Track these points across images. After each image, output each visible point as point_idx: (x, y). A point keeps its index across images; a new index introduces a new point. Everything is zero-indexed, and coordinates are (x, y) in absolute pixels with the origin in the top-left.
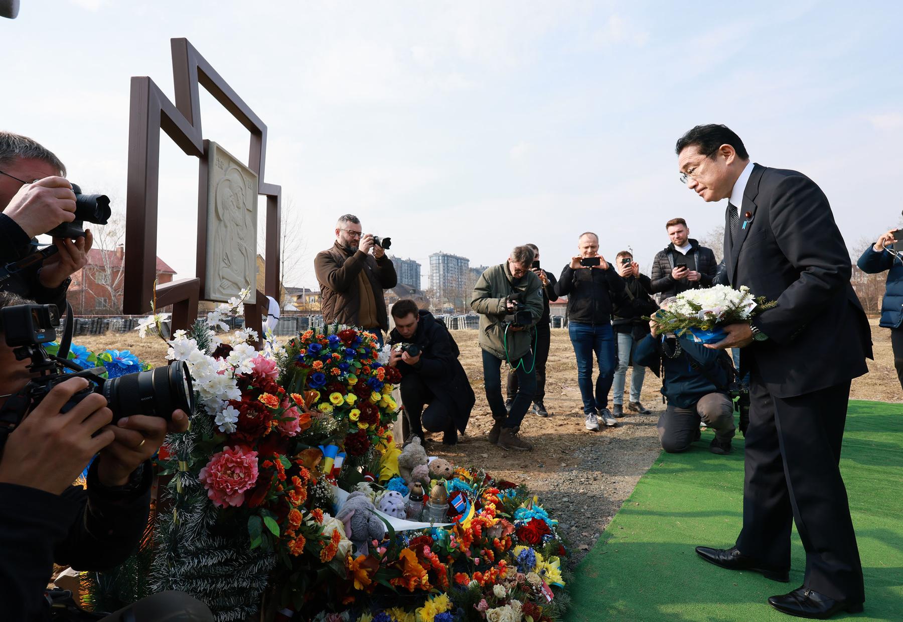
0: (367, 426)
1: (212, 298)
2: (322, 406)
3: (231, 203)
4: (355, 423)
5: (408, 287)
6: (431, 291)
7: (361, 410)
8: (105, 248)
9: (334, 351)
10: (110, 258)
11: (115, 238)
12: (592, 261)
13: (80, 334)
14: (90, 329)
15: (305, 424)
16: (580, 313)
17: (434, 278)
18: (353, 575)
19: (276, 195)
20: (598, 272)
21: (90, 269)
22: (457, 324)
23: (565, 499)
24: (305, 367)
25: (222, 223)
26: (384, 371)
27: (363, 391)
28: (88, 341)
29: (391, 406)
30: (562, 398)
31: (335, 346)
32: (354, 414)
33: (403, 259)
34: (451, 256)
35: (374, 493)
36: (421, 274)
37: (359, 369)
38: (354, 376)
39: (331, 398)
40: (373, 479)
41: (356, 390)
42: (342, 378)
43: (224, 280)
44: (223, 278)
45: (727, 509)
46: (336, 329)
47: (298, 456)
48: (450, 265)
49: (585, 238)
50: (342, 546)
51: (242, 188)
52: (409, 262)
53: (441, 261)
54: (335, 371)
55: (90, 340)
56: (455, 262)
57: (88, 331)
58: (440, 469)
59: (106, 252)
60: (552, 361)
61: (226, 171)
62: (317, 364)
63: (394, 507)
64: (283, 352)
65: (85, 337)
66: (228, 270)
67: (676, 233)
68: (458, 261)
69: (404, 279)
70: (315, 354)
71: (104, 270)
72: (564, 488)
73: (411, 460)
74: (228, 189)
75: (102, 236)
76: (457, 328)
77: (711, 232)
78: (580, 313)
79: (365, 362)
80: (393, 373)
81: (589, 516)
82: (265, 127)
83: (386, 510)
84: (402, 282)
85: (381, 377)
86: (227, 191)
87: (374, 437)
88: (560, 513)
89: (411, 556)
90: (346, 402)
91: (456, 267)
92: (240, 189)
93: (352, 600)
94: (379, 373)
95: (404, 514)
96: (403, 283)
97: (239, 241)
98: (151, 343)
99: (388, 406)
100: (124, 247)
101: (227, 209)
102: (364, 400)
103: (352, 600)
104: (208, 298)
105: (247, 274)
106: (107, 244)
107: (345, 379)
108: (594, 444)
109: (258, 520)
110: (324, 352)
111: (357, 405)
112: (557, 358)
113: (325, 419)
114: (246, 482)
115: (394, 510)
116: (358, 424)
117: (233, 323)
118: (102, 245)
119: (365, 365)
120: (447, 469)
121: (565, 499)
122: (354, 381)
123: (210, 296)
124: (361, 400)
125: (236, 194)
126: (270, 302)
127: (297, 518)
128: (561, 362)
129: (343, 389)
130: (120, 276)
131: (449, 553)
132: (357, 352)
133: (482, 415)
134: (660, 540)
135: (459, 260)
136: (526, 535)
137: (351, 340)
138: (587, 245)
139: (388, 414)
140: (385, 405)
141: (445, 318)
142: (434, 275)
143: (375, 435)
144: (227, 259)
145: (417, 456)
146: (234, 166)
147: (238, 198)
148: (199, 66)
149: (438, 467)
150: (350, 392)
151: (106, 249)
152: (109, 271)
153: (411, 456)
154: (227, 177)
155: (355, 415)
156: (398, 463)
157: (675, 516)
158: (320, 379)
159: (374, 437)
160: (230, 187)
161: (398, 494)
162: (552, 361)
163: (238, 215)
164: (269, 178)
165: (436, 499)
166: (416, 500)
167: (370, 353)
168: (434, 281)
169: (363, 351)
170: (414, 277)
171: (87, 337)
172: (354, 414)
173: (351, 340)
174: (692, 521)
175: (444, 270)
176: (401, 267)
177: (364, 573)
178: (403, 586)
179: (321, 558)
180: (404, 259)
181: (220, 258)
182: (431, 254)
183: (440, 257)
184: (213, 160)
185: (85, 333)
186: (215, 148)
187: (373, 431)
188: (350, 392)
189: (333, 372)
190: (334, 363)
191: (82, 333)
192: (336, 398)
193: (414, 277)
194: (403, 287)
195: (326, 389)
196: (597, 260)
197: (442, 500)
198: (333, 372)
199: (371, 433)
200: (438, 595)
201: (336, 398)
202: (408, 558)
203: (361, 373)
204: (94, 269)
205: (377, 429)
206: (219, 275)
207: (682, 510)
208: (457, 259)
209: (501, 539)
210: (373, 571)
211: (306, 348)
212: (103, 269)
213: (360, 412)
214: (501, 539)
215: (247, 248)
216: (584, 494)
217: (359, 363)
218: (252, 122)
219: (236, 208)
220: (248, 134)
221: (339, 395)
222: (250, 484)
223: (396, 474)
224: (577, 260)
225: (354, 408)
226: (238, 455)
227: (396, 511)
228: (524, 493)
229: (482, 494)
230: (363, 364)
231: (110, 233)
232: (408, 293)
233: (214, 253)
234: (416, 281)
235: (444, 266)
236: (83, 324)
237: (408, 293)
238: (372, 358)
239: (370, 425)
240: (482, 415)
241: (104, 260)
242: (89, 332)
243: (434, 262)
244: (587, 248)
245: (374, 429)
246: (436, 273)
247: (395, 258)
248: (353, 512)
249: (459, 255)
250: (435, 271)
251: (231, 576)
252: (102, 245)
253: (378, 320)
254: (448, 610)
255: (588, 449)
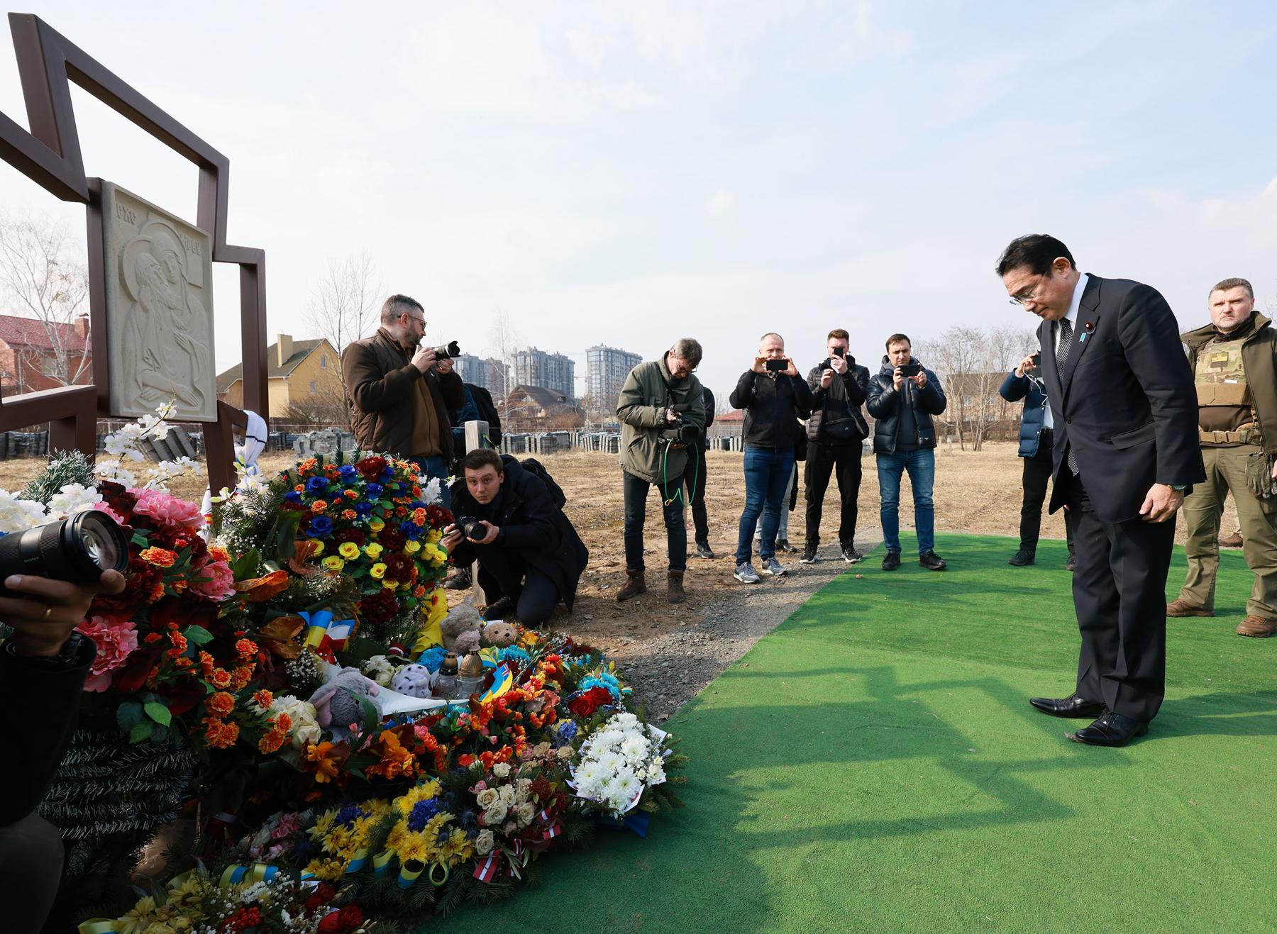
0: (397, 584)
1: (122, 414)
2: (327, 561)
3: (155, 276)
4: (379, 582)
5: (555, 393)
6: (589, 400)
7: (387, 564)
8: (50, 318)
9: (350, 487)
10: (61, 336)
11: (69, 304)
12: (778, 364)
13: (15, 457)
14: (34, 449)
15: (280, 584)
16: (761, 435)
17: (594, 381)
18: (315, 766)
19: (253, 262)
20: (783, 378)
21: (27, 352)
22: (617, 446)
23: (665, 664)
24: (297, 508)
25: (138, 306)
26: (425, 513)
27: (393, 541)
28: (26, 467)
29: (438, 558)
30: (720, 542)
31: (350, 480)
32: (377, 571)
33: (548, 353)
34: (617, 352)
35: (393, 668)
36: (575, 375)
37: (392, 510)
38: (379, 520)
39: (342, 550)
40: (402, 652)
41: (382, 538)
42: (360, 522)
43: (148, 388)
44: (145, 385)
45: (845, 666)
46: (357, 457)
47: (268, 627)
48: (616, 364)
49: (769, 339)
50: (303, 733)
51: (178, 254)
52: (557, 357)
53: (602, 358)
54: (348, 513)
55: (29, 466)
56: (622, 359)
57: (29, 451)
58: (498, 635)
59: (55, 327)
60: (726, 496)
61: (140, 227)
62: (318, 505)
63: (412, 683)
64: (263, 490)
65: (24, 461)
66: (157, 374)
67: (1227, 304)
68: (626, 360)
69: (550, 381)
70: (319, 491)
71: (53, 355)
72: (669, 651)
73: (458, 625)
74: (148, 255)
75: (45, 300)
76: (617, 452)
77: (945, 333)
78: (761, 435)
79: (400, 501)
80: (441, 515)
81: (686, 682)
82: (226, 162)
83: (400, 688)
84: (547, 387)
85: (420, 521)
86: (145, 257)
87: (408, 598)
88: (652, 680)
89: (392, 740)
90: (364, 555)
91: (624, 367)
92: (172, 255)
93: (316, 795)
94: (417, 515)
95: (427, 691)
96: (550, 387)
97: (176, 331)
98: (139, 471)
99: (433, 558)
100: (89, 318)
101: (146, 284)
102: (394, 551)
103: (316, 795)
104: (117, 415)
105: (195, 379)
106: (55, 313)
107: (364, 523)
108: (729, 598)
109: (137, 707)
110: (333, 488)
111: (383, 557)
112: (732, 491)
113: (317, 577)
114: (109, 661)
115: (411, 688)
116: (384, 582)
117: (284, 441)
118: (46, 315)
119: (400, 505)
120: (507, 635)
121: (665, 664)
122: (378, 526)
123: (118, 412)
124: (390, 551)
125: (165, 262)
126: (249, 419)
127: (225, 702)
128: (737, 497)
129: (362, 537)
130: (85, 366)
131: (454, 733)
132: (385, 488)
133: (606, 566)
134: (753, 703)
135: (628, 358)
136: (579, 707)
137: (377, 472)
138: (771, 347)
139: (434, 568)
140: (428, 558)
141: (527, 438)
142: (594, 377)
143: (411, 596)
144: (153, 359)
145: (466, 620)
146: (155, 219)
147: (168, 268)
148: (70, 61)
149: (496, 633)
150: (374, 540)
151: (53, 321)
152: (62, 358)
153: (458, 620)
154: (144, 236)
155: (379, 571)
156: (439, 629)
157: (783, 676)
158: (324, 526)
159: (408, 598)
160: (151, 251)
161: (420, 668)
162: (726, 496)
163: (170, 293)
164: (234, 238)
165: (466, 671)
166: (447, 674)
167: (409, 489)
168: (594, 386)
169: (396, 487)
170: (565, 379)
171: (29, 460)
172: (377, 571)
173: (377, 472)
174: (799, 681)
175: (607, 370)
176: (546, 365)
177: (329, 763)
178: (380, 774)
179: (260, 749)
180: (550, 353)
181: (136, 356)
182: (589, 347)
183: (602, 353)
184: (109, 209)
185: (25, 455)
186: (113, 193)
187: (407, 592)
188: (373, 542)
189: (345, 515)
190: (347, 502)
191: (21, 455)
192: (349, 550)
193: (565, 379)
194: (547, 393)
195: (333, 538)
196: (784, 363)
197: (474, 672)
198: (345, 515)
199: (404, 594)
200: (430, 780)
201: (349, 550)
202: (389, 742)
203: (394, 515)
204: (34, 352)
205: (413, 589)
206: (136, 381)
207: (797, 669)
208: (626, 355)
209: (539, 714)
210: (342, 760)
211: (305, 483)
212: (50, 353)
213: (386, 567)
214: (539, 714)
215: (194, 342)
216: (692, 656)
217: (390, 503)
218: (197, 153)
219: (166, 283)
220: (194, 169)
221: (353, 545)
222: (113, 664)
223: (437, 644)
224: (760, 361)
225: (379, 562)
226: (96, 628)
227: (413, 689)
228: (597, 658)
229: (537, 662)
230: (395, 504)
231: (58, 295)
232: (555, 401)
233: (124, 349)
234: (568, 385)
235: (607, 366)
236: (19, 441)
237: (555, 401)
238: (411, 496)
239: (401, 583)
240: (606, 566)
241: (51, 338)
242: (32, 453)
243: (593, 359)
244: (771, 351)
245: (409, 588)
246: (596, 374)
247: (538, 352)
248: (334, 692)
249: (628, 350)
250: (594, 372)
251: (112, 778)
252: (46, 315)
253: (441, 447)
254: (435, 796)
255: (720, 603)
